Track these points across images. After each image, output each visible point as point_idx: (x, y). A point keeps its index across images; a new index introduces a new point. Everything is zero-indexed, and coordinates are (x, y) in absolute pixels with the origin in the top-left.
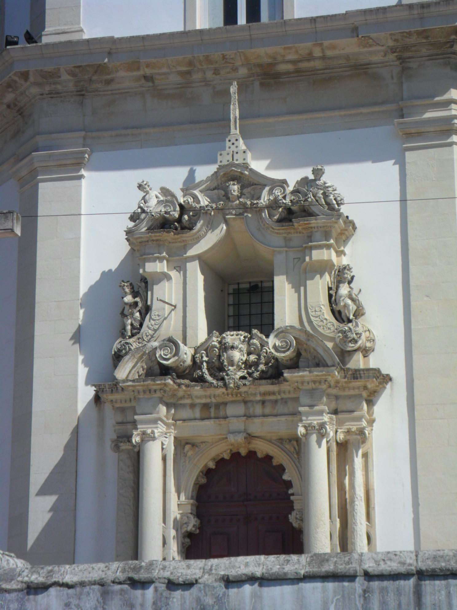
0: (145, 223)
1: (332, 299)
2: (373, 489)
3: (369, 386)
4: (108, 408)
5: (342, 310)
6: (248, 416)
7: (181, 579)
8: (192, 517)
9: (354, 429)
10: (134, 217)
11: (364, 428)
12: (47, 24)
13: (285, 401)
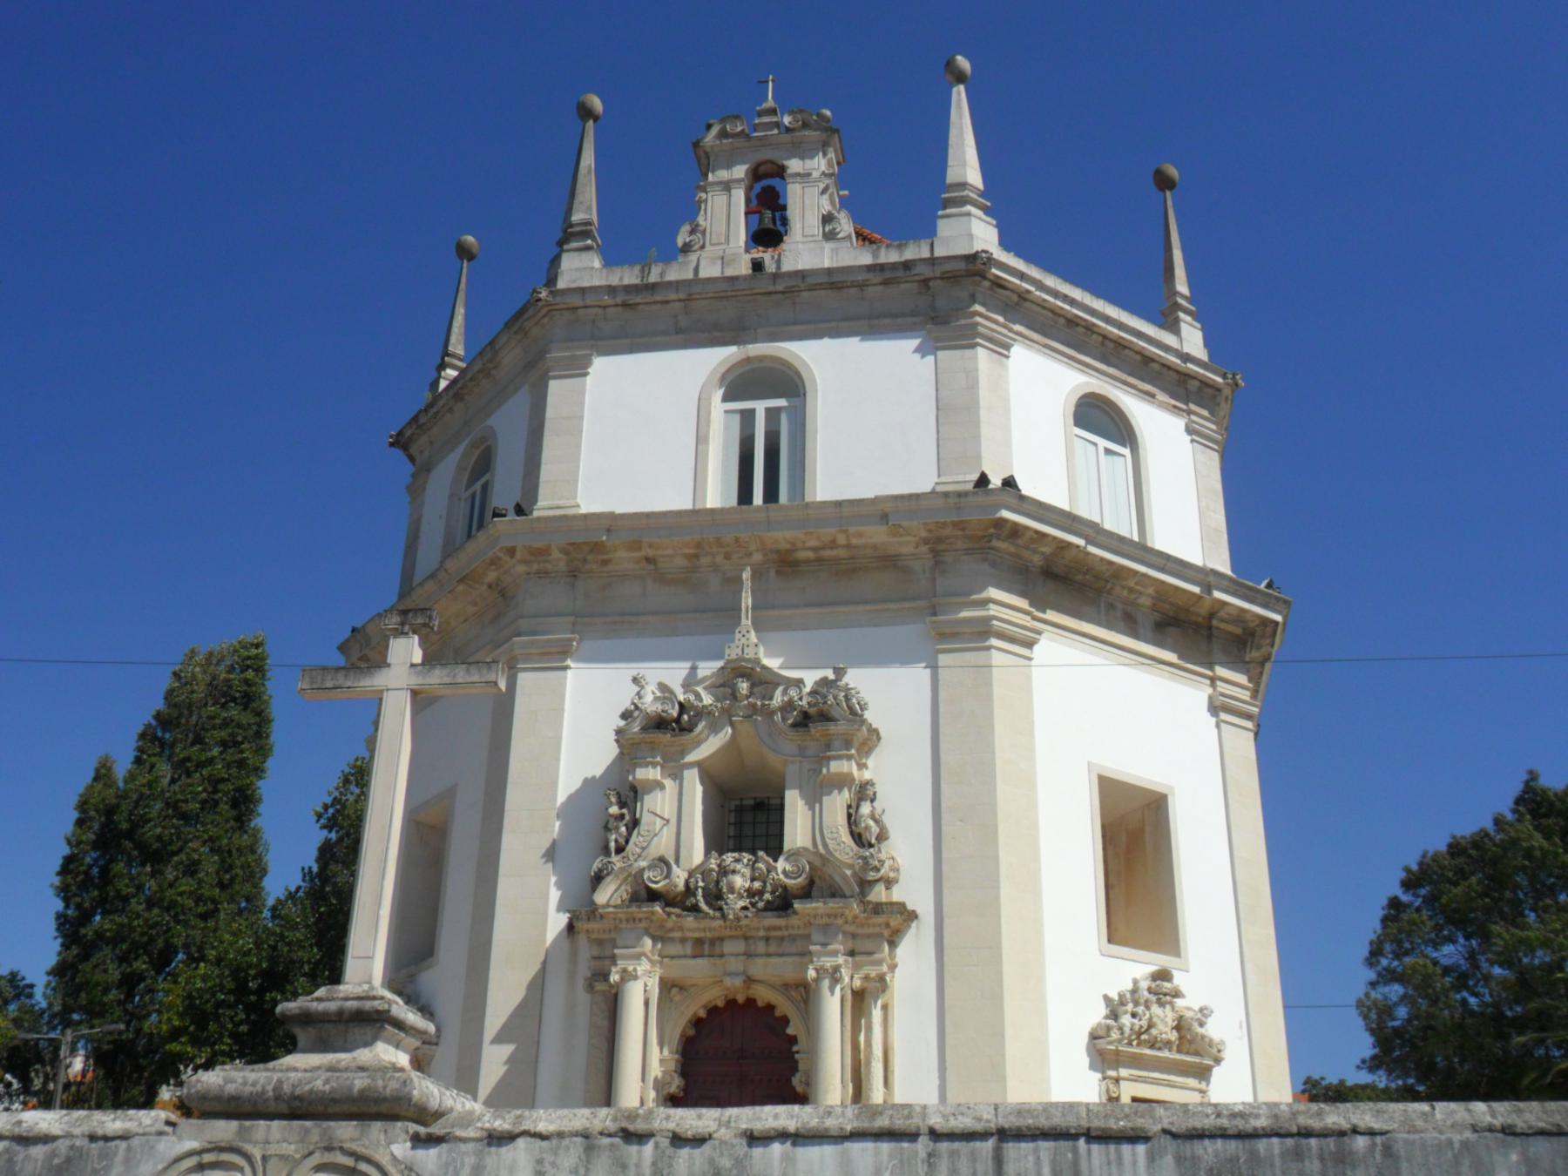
0: (638, 721)
1: (852, 819)
2: (893, 1049)
3: (893, 923)
4: (582, 940)
5: (863, 832)
6: (749, 955)
7: (689, 1133)
8: (675, 1075)
9: (873, 974)
10: (626, 715)
11: (885, 974)
12: (540, 498)
13: (793, 939)
